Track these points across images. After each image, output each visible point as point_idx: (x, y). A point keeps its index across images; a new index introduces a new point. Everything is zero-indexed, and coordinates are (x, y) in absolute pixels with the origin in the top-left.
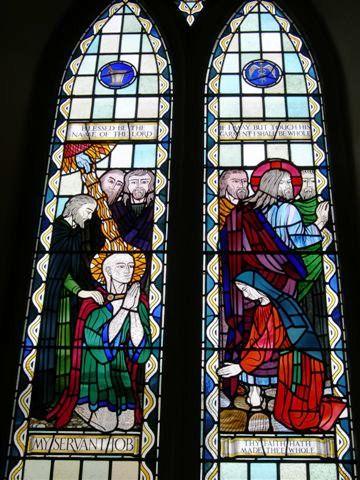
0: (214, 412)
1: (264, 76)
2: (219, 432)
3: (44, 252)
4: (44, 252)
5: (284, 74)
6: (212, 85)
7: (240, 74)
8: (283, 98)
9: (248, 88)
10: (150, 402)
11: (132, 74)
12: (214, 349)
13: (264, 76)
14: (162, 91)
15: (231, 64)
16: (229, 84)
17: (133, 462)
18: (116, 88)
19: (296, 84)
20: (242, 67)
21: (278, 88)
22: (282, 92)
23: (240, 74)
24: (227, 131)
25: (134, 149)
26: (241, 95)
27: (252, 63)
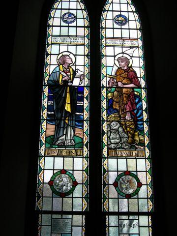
0: (85, 149)
1: (122, 21)
2: (45, 147)
3: (86, 98)
4: (86, 98)
5: (129, 20)
6: (103, 24)
7: (113, 20)
8: (128, 30)
9: (116, 26)
10: (86, 151)
11: (126, 20)
12: (45, 120)
13: (69, 18)
14: (138, 28)
15: (58, 14)
16: (109, 24)
17: (67, 169)
18: (68, 23)
19: (80, 22)
20: (114, 16)
21: (126, 26)
22: (128, 28)
23: (113, 20)
24: (109, 42)
25: (111, 56)
26: (113, 28)
27: (66, 14)
